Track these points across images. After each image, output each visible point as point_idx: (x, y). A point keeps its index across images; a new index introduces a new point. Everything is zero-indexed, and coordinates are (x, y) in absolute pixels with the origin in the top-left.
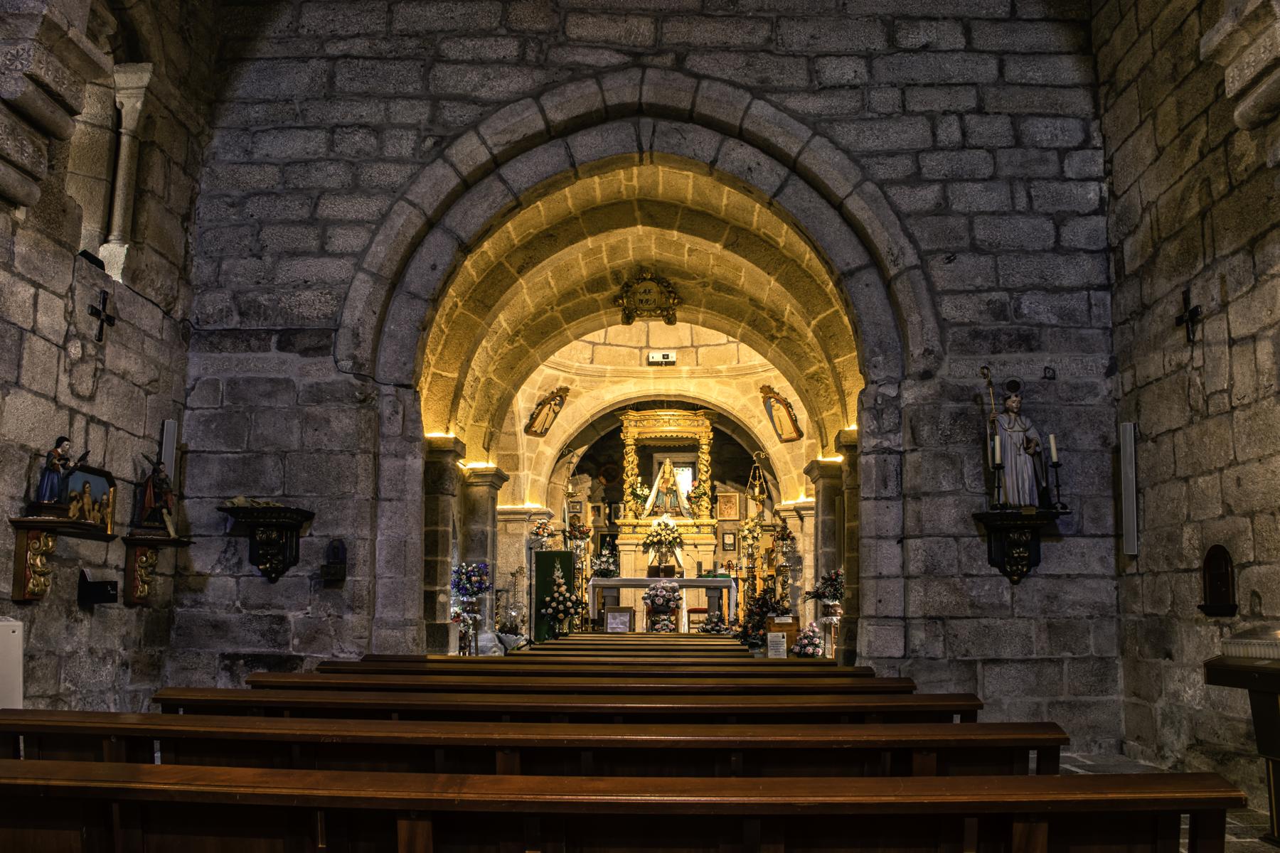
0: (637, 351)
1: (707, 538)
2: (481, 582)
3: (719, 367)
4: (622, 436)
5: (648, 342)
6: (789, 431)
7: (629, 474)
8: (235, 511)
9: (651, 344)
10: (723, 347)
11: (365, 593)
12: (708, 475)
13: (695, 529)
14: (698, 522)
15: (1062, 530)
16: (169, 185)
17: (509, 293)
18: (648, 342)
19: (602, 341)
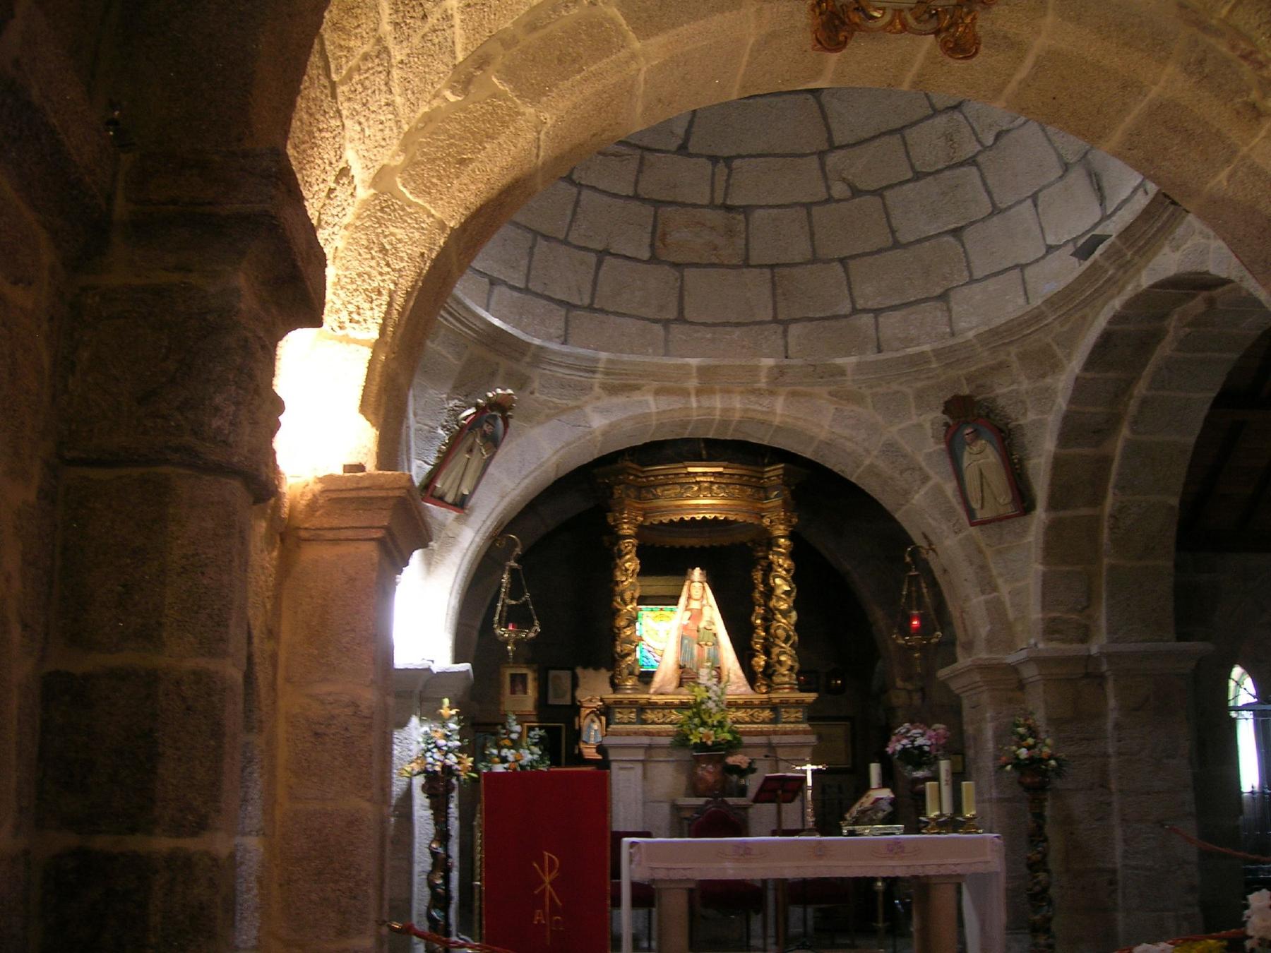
0: (658, 328)
1: (796, 732)
2: (628, 91)
3: (839, 361)
4: (610, 520)
5: (681, 310)
6: (1000, 498)
7: (627, 596)
8: (1018, 764)
9: (689, 315)
10: (843, 322)
11: (1111, 375)
12: (791, 601)
13: (767, 714)
14: (776, 696)
15: (567, 701)
16: (168, 460)
17: (382, 412)
18: (681, 310)
19: (587, 301)
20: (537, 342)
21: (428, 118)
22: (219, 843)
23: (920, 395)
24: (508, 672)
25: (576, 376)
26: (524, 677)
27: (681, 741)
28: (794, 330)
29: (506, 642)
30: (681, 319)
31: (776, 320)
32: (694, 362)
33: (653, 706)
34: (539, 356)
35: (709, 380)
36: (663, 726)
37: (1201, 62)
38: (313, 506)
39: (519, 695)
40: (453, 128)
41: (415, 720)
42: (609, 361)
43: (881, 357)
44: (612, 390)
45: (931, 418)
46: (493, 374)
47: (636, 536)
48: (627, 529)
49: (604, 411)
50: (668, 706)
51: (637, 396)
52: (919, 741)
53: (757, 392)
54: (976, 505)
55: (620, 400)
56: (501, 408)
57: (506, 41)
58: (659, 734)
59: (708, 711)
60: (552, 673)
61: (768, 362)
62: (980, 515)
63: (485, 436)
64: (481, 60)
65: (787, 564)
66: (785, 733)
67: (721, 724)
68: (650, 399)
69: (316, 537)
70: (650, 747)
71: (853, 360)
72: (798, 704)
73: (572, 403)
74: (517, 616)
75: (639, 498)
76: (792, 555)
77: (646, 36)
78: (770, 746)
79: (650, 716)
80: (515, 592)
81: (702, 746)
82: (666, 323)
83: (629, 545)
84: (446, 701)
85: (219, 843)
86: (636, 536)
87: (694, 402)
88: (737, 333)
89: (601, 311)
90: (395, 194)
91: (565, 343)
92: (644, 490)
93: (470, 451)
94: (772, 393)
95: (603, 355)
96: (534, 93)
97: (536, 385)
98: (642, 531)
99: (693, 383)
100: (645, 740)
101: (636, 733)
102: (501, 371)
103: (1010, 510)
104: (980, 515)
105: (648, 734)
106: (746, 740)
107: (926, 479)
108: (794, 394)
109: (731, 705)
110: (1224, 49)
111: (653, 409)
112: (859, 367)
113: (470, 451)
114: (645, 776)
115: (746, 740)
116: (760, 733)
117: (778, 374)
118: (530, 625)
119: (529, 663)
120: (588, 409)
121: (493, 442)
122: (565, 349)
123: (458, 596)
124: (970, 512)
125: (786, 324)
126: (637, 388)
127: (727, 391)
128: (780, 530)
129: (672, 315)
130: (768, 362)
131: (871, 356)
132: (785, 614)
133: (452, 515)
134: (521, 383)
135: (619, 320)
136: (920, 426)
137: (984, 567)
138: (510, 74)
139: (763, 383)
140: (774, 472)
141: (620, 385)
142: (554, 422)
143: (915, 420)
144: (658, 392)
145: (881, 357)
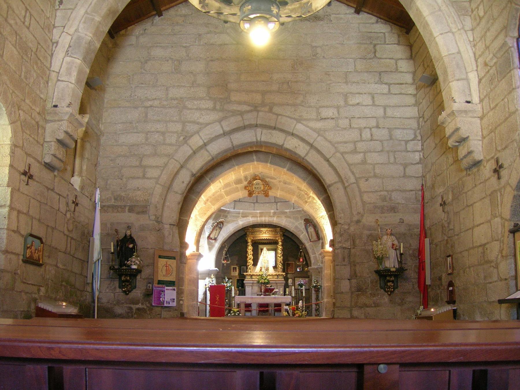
1: (281, 280)
3: (286, 211)
7: (249, 254)
9: (258, 202)
13: (276, 277)
20: (228, 210)
21: (201, 208)
22: (183, 288)
23: (301, 217)
24: (232, 267)
25: (236, 215)
26: (236, 268)
27: (258, 282)
28: (279, 204)
29: (224, 264)
30: (257, 202)
31: (275, 202)
32: (258, 211)
33: (254, 275)
34: (229, 212)
35: (261, 215)
36: (255, 279)
37: (299, 195)
38: (189, 256)
39: (235, 272)
40: (204, 209)
41: (207, 278)
42: (242, 212)
43: (294, 210)
44: (243, 217)
45: (303, 222)
46: (220, 216)
47: (252, 242)
48: (249, 241)
49: (241, 221)
50: (257, 275)
51: (248, 218)
52: (302, 282)
53: (271, 217)
54: (311, 238)
55: (245, 218)
56: (222, 223)
57: (210, 197)
58: (255, 281)
59: (263, 276)
60: (242, 267)
61: (272, 211)
62: (312, 240)
63: (219, 227)
64: (207, 200)
65: (281, 247)
66: (279, 281)
67: (266, 279)
68: (250, 218)
69: (189, 259)
70: (253, 283)
71: (288, 210)
72: (282, 275)
73: (236, 219)
74: (226, 259)
75: (252, 234)
76: (282, 245)
77: (227, 196)
78: (276, 283)
79: (253, 277)
80: (226, 255)
81: (262, 283)
82: (254, 203)
83: (250, 244)
84: (212, 275)
85: (183, 288)
86: (252, 242)
87: (259, 219)
88: (268, 204)
89: (241, 201)
90: (197, 218)
91: (234, 209)
92: (253, 233)
93: (216, 230)
94: (274, 217)
95: (241, 211)
96: (214, 204)
97: (229, 216)
98: (252, 241)
99: (258, 215)
100: (252, 282)
101: (250, 280)
102: (222, 215)
103: (317, 239)
104: (312, 240)
105: (252, 280)
106: (271, 282)
107: (303, 233)
108: (278, 217)
109: (269, 275)
110: (303, 193)
111: (251, 220)
112: (289, 212)
113: (216, 230)
114: (252, 288)
115: (271, 282)
116: (275, 281)
117: (275, 213)
118: (228, 261)
119: (237, 265)
120: (239, 220)
121: (221, 228)
122: (234, 210)
123: (247, 223)
124: (310, 240)
125: (277, 203)
126: (248, 216)
127: (265, 216)
128: (280, 241)
129: (255, 201)
130: (272, 211)
131: (292, 210)
132: (280, 257)
133: (214, 241)
134: (226, 217)
135: (245, 203)
136: (301, 223)
137: (313, 250)
138: (211, 202)
139: (272, 215)
140: (278, 229)
141: (245, 216)
142: (232, 223)
143: (300, 222)
144: (252, 217)
145: (294, 210)
